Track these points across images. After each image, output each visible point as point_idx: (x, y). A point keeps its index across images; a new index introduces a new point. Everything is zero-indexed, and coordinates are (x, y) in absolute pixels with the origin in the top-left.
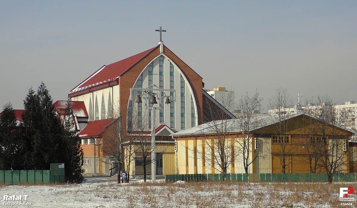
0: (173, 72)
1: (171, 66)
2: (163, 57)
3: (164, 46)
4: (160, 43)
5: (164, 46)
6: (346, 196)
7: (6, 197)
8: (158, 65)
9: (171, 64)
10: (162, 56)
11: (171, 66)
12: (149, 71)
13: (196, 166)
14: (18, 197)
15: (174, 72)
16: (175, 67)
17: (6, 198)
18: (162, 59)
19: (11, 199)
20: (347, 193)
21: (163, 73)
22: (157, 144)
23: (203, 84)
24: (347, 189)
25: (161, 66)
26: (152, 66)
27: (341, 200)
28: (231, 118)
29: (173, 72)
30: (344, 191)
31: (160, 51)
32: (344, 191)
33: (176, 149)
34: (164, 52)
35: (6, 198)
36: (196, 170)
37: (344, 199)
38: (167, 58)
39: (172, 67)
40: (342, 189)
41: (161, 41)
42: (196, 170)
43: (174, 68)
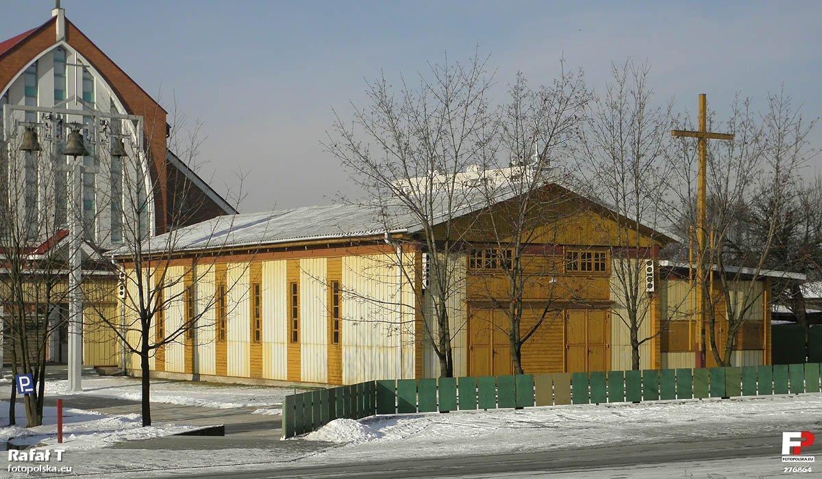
0: (62, 91)
1: (87, 75)
2: (65, 50)
3: (67, 22)
4: (55, 13)
5: (67, 22)
6: (794, 451)
7: (13, 453)
8: (51, 72)
9: (85, 71)
10: (61, 48)
11: (87, 75)
12: (26, 87)
13: (193, 340)
14: (42, 454)
15: (93, 91)
16: (98, 79)
17: (15, 456)
18: (60, 57)
19: (26, 459)
20: (798, 444)
21: (64, 93)
22: (85, 280)
23: (168, 127)
24: (798, 435)
25: (59, 76)
26: (35, 72)
27: (784, 461)
28: (226, 214)
29: (62, 91)
30: (792, 439)
31: (57, 33)
32: (792, 439)
33: (121, 293)
34: (67, 38)
35: (15, 456)
36: (294, 362)
37: (793, 457)
38: (74, 56)
39: (87, 79)
40: (787, 436)
41: (58, 6)
42: (294, 362)
43: (93, 81)
